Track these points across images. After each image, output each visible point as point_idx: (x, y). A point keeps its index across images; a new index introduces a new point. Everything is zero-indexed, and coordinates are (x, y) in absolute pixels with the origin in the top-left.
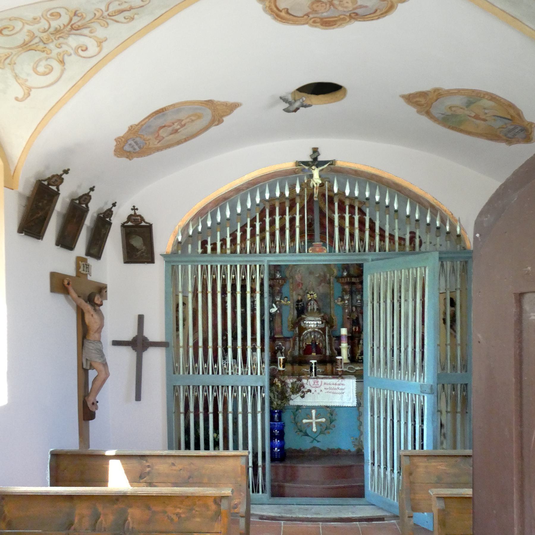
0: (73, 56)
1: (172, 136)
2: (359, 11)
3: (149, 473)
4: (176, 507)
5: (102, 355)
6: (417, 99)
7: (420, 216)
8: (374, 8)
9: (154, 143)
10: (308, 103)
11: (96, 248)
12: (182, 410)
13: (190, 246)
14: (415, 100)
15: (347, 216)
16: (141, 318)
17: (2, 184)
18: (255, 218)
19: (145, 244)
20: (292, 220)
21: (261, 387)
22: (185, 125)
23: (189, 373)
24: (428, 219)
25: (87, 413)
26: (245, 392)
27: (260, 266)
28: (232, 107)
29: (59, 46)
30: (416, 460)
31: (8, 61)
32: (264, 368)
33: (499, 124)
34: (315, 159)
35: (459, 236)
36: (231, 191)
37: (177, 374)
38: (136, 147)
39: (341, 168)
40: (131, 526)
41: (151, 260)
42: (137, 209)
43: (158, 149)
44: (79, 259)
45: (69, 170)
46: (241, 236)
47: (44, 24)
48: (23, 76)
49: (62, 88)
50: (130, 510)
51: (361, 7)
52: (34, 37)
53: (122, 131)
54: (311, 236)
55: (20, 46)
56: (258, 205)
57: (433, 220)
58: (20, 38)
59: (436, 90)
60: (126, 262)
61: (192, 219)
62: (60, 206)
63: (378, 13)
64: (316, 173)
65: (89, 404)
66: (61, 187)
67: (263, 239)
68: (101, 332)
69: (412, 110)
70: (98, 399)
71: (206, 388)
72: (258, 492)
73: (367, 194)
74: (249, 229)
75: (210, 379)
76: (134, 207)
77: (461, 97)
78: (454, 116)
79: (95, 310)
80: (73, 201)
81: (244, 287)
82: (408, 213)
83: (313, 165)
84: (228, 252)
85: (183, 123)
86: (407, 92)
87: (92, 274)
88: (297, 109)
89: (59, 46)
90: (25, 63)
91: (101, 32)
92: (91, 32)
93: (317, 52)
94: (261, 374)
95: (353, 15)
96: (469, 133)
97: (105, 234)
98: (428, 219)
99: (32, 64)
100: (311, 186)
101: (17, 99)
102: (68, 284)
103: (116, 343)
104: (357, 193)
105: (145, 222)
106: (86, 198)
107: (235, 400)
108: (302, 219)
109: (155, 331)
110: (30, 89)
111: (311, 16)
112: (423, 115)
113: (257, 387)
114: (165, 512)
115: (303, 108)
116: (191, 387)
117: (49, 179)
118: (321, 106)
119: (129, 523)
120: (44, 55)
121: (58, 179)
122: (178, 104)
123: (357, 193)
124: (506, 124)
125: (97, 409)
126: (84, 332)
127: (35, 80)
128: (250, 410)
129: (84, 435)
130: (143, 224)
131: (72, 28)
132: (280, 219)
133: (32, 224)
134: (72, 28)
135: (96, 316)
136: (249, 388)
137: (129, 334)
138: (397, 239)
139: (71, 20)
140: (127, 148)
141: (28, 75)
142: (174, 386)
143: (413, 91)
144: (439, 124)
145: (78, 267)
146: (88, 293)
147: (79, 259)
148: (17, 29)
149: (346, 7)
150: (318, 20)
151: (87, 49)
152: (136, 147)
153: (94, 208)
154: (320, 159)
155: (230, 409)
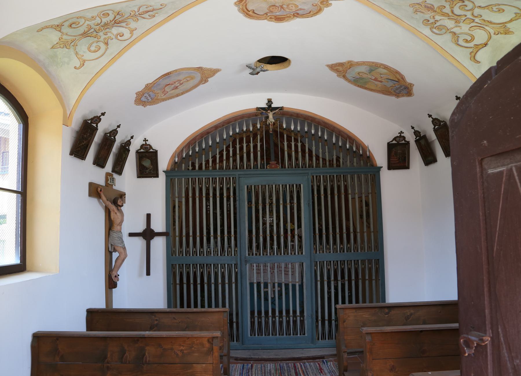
2: (299, 12)
4: (180, 345)
5: (123, 242)
6: (337, 68)
8: (310, 10)
9: (161, 96)
10: (265, 68)
11: (118, 168)
12: (178, 281)
13: (183, 165)
14: (335, 68)
15: (286, 143)
16: (149, 216)
17: (62, 123)
18: (229, 145)
19: (152, 164)
20: (255, 147)
21: (235, 265)
22: (182, 83)
23: (183, 255)
25: (111, 283)
27: (233, 178)
28: (214, 72)
29: (106, 34)
30: (347, 311)
31: (72, 44)
32: (236, 251)
33: (390, 84)
34: (270, 106)
35: (369, 157)
36: (212, 128)
37: (174, 256)
38: (149, 98)
39: (287, 112)
41: (157, 176)
42: (147, 140)
43: (164, 100)
45: (105, 113)
46: (220, 158)
47: (98, 20)
48: (81, 53)
49: (104, 60)
50: (147, 348)
51: (301, 9)
52: (91, 28)
53: (141, 87)
54: (269, 159)
55: (81, 35)
56: (231, 136)
57: (351, 147)
58: (81, 30)
59: (349, 62)
60: (138, 177)
62: (98, 138)
63: (312, 13)
65: (113, 277)
66: (99, 125)
67: (235, 161)
68: (121, 225)
69: (334, 75)
70: (119, 273)
71: (195, 266)
74: (225, 153)
75: (199, 259)
76: (145, 139)
77: (366, 66)
78: (361, 78)
79: (118, 209)
81: (221, 195)
84: (211, 168)
85: (181, 82)
87: (116, 185)
88: (259, 72)
89: (106, 34)
90: (83, 46)
91: (133, 25)
92: (127, 25)
93: (272, 37)
94: (235, 255)
95: (295, 14)
96: (371, 90)
99: (87, 45)
100: (268, 123)
101: (75, 68)
102: (101, 191)
103: (131, 235)
104: (299, 128)
105: (152, 149)
108: (262, 146)
110: (84, 61)
111: (269, 14)
113: (232, 265)
114: (172, 349)
116: (184, 265)
117: (92, 119)
118: (273, 72)
119: (146, 358)
120: (96, 39)
121: (97, 119)
123: (299, 128)
124: (395, 84)
125: (118, 280)
126: (111, 226)
127: (88, 56)
128: (227, 281)
130: (151, 150)
131: (115, 23)
132: (247, 146)
133: (79, 150)
134: (115, 23)
135: (118, 214)
136: (226, 265)
137: (141, 228)
139: (115, 18)
140: (143, 99)
141: (84, 52)
142: (172, 265)
144: (352, 83)
145: (107, 180)
146: (113, 199)
147: (107, 174)
148: (81, 24)
149: (291, 10)
150: (273, 17)
151: (123, 35)
152: (149, 98)
153: (119, 139)
154: (273, 106)
155: (213, 281)
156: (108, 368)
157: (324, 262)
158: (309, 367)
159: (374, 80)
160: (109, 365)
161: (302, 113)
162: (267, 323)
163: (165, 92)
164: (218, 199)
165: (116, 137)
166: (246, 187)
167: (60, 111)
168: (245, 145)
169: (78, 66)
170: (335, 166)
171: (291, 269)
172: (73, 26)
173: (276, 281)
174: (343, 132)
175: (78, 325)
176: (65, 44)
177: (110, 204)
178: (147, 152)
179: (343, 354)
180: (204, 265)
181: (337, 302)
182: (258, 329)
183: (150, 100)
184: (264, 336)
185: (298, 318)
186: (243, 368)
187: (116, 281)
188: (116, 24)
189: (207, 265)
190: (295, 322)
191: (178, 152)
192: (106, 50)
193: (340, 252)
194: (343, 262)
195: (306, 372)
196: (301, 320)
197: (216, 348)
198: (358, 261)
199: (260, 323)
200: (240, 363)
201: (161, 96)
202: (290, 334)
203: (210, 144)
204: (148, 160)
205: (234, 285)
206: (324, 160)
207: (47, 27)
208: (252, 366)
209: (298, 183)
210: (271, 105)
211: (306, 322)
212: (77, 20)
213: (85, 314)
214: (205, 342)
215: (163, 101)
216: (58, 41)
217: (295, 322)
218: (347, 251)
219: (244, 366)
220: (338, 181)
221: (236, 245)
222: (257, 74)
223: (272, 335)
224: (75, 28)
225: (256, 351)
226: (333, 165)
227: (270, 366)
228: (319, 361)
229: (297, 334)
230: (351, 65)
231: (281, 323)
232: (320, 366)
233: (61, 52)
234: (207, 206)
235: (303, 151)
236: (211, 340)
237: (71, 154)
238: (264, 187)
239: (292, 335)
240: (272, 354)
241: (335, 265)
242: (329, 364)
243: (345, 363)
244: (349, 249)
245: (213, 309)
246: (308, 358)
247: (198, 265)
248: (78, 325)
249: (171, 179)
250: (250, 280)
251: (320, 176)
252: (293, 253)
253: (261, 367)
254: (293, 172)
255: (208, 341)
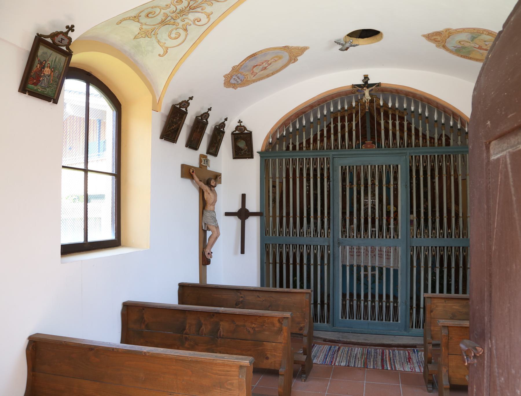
0: (192, 25)
1: (262, 72)
3: (242, 302)
4: (252, 323)
5: (216, 221)
6: (435, 37)
7: (445, 121)
9: (250, 77)
11: (214, 148)
13: (277, 146)
14: (433, 38)
15: (390, 122)
16: (244, 196)
19: (247, 145)
21: (327, 246)
22: (271, 64)
24: (451, 123)
25: (205, 260)
26: (315, 249)
27: (327, 159)
28: (302, 50)
29: (183, 20)
30: (436, 301)
31: (153, 33)
32: (329, 233)
36: (306, 107)
38: (238, 80)
39: (385, 88)
40: (222, 334)
41: (252, 157)
43: (254, 81)
44: (202, 156)
45: (193, 97)
47: (173, 8)
48: (163, 41)
49: (187, 46)
50: (221, 323)
52: (167, 16)
53: (228, 70)
54: (364, 137)
55: (160, 23)
57: (455, 124)
58: (159, 18)
59: (447, 30)
61: (279, 128)
64: (367, 92)
65: (206, 254)
66: (188, 109)
69: (432, 45)
71: (309, 247)
72: (324, 322)
73: (405, 106)
75: (292, 240)
77: (467, 34)
78: (464, 48)
79: (211, 190)
80: (197, 117)
81: (322, 175)
82: (436, 119)
83: (365, 87)
84: (304, 149)
85: (269, 62)
86: (426, 33)
89: (183, 20)
90: (163, 33)
92: (202, 10)
94: (327, 237)
97: (220, 139)
98: (451, 123)
100: (364, 101)
101: (159, 55)
102: (193, 172)
103: (227, 214)
104: (397, 105)
106: (206, 115)
107: (309, 255)
109: (253, 205)
110: (167, 48)
112: (441, 48)
113: (324, 246)
115: (353, 47)
117: (180, 104)
118: (365, 46)
119: (220, 332)
120: (174, 27)
121: (186, 104)
122: (264, 50)
126: (204, 205)
127: (170, 43)
129: (203, 274)
130: (246, 132)
131: (190, 9)
133: (169, 133)
134: (190, 9)
135: (211, 194)
136: (319, 247)
137: (236, 207)
138: (428, 137)
139: (189, 4)
140: (232, 81)
141: (166, 40)
142: (266, 244)
143: (430, 31)
144: (454, 54)
145: (201, 161)
147: (202, 156)
148: (157, 13)
151: (200, 20)
152: (238, 80)
154: (369, 82)
156: (186, 338)
157: (421, 247)
158: (397, 355)
159: (478, 48)
160: (187, 336)
161: (401, 88)
162: (359, 306)
163: (254, 74)
164: (319, 180)
165: (208, 120)
166: (340, 167)
167: (150, 97)
168: (346, 124)
169: (162, 53)
170: (436, 145)
171: (390, 253)
172: (150, 15)
173: (370, 264)
174: (447, 108)
175: (170, 298)
176: (147, 34)
177: (203, 184)
178: (242, 133)
179: (428, 345)
180: (296, 245)
181: (426, 291)
182: (350, 312)
183: (240, 82)
184: (355, 319)
185: (392, 304)
186: (330, 350)
187: (209, 258)
188: (191, 10)
189: (300, 245)
190: (388, 308)
191: (272, 133)
192: (186, 36)
193: (439, 237)
194: (442, 249)
195: (394, 360)
196: (394, 307)
197: (285, 328)
198: (459, 247)
199: (351, 307)
200: (328, 345)
201: (252, 78)
202: (382, 320)
203: (304, 124)
204: (242, 141)
205: (326, 267)
206: (424, 136)
207: (125, 19)
208: (339, 348)
209: (395, 164)
210: (367, 82)
211: (399, 308)
212: (153, 10)
213: (177, 287)
214: (276, 321)
215: (254, 82)
216: (138, 31)
217: (388, 308)
218: (447, 237)
219: (331, 347)
220: (439, 161)
221: (329, 228)
222: (347, 49)
223: (364, 319)
224: (152, 17)
225: (346, 334)
226: (434, 143)
227: (358, 350)
228: (410, 350)
229: (390, 321)
230: (449, 33)
231: (373, 307)
232: (409, 355)
233: (144, 41)
234: (309, 186)
235: (409, 129)
236: (281, 320)
237: (161, 138)
238: (358, 168)
239: (384, 321)
240: (361, 339)
241: (434, 251)
242: (420, 353)
243: (429, 355)
244: (450, 235)
245: (298, 290)
246: (398, 346)
247: (291, 246)
248: (170, 298)
249: (266, 160)
250: (342, 262)
251: (419, 156)
252: (388, 237)
253: (349, 350)
254: (390, 152)
255: (279, 320)
